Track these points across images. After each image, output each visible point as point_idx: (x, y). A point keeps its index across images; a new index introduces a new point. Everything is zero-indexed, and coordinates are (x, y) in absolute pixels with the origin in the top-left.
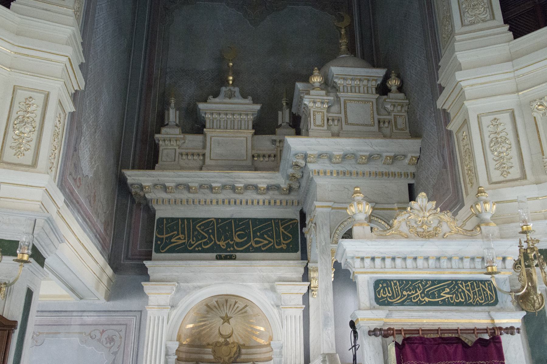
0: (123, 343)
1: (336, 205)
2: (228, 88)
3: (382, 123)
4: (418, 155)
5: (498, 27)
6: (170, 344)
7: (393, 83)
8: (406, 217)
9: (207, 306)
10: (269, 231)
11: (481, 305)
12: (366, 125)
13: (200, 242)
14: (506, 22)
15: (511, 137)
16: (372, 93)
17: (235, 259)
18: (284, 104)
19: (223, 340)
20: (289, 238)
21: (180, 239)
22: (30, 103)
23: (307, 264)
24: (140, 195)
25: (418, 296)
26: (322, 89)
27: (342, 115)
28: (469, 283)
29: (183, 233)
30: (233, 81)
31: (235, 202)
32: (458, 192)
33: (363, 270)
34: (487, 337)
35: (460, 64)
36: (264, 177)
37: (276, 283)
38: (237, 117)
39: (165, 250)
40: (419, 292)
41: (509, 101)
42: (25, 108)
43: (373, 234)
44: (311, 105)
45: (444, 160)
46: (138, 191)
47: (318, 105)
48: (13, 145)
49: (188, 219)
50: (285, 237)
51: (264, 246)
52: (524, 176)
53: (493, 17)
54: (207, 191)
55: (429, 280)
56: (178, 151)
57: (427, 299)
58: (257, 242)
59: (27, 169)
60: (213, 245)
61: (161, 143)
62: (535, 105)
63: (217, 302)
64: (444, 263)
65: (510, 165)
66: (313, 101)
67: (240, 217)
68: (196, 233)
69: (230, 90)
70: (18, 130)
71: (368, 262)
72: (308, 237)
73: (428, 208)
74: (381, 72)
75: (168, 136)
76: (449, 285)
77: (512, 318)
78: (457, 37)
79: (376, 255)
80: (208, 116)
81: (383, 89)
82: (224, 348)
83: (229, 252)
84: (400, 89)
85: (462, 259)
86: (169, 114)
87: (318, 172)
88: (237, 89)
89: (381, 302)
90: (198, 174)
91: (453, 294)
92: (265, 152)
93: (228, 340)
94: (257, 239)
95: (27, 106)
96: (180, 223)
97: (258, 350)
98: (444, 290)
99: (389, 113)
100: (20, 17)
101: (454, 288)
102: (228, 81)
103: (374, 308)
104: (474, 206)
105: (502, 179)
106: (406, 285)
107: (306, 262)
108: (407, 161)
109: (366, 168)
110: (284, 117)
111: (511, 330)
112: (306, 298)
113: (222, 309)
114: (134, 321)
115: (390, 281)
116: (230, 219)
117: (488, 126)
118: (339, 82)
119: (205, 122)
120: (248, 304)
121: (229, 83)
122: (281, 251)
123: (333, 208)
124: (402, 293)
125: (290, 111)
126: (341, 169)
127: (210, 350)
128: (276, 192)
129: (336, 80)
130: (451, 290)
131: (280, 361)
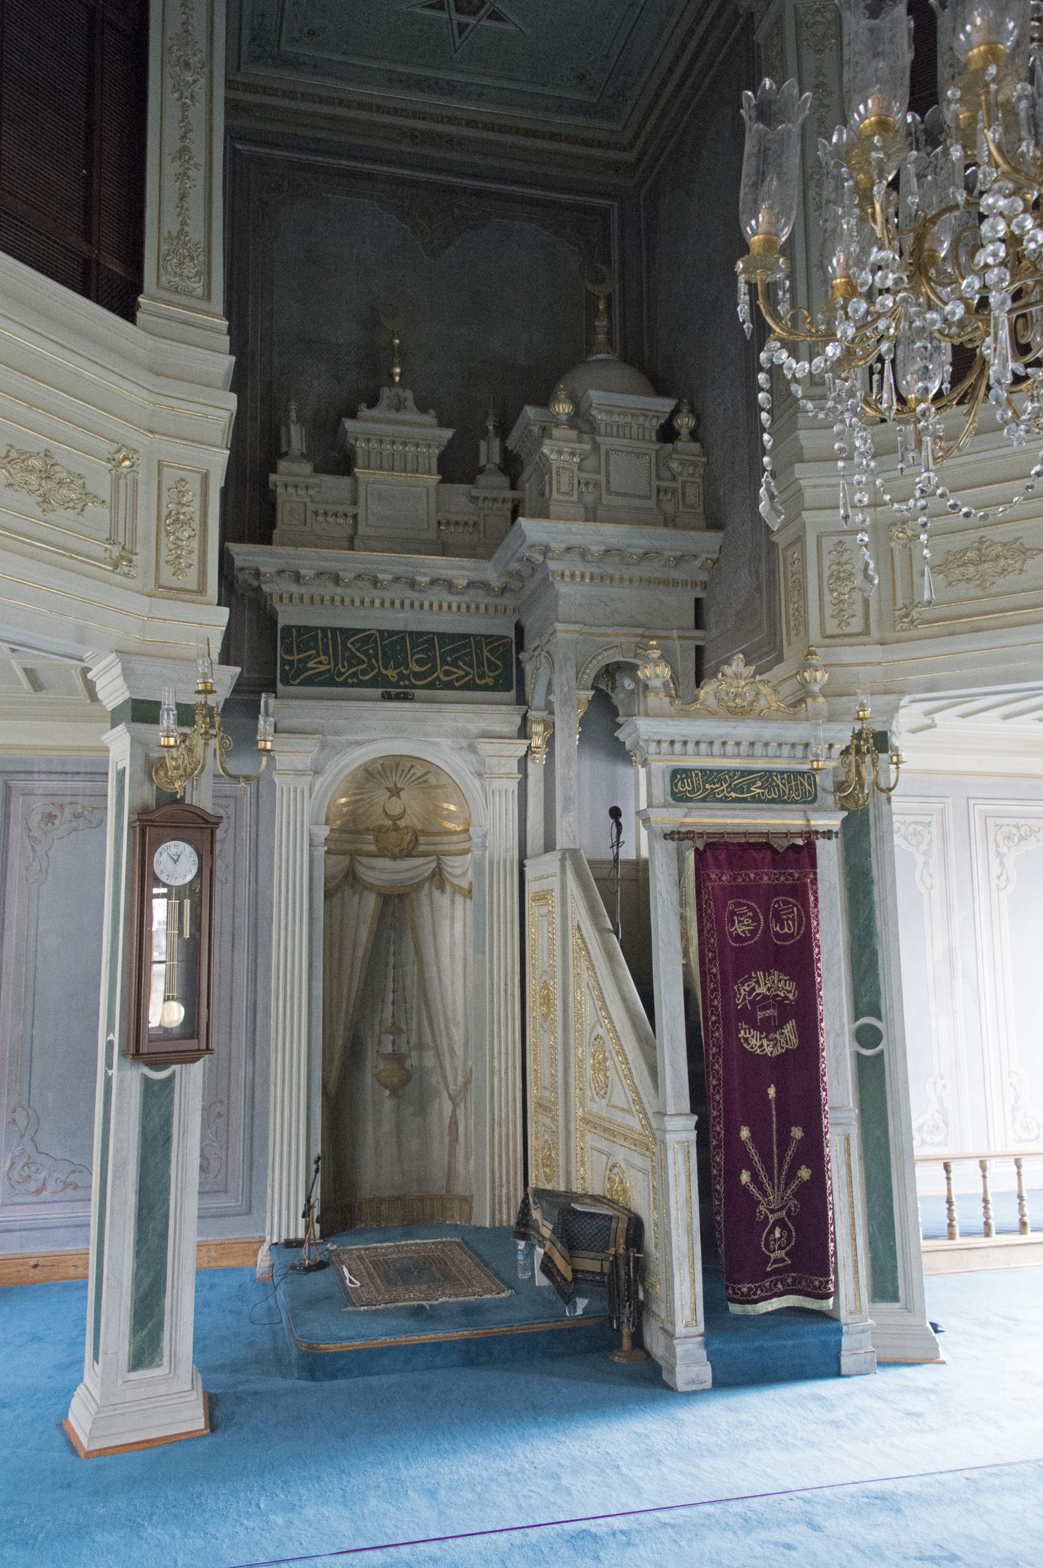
3: (662, 494)
4: (715, 556)
6: (316, 829)
7: (685, 422)
9: (366, 770)
10: (466, 654)
11: (796, 802)
16: (651, 441)
18: (491, 428)
19: (391, 822)
20: (497, 667)
21: (321, 663)
27: (602, 478)
28: (785, 775)
29: (326, 653)
30: (401, 375)
31: (412, 605)
32: (775, 634)
34: (800, 842)
37: (481, 740)
38: (411, 449)
39: (298, 681)
40: (725, 786)
44: (553, 456)
45: (758, 579)
46: (250, 580)
48: (170, 558)
49: (334, 630)
50: (493, 667)
51: (458, 679)
52: (866, 632)
54: (368, 585)
56: (311, 507)
57: (733, 795)
58: (447, 673)
60: (374, 676)
62: (895, 532)
63: (382, 765)
64: (759, 749)
65: (851, 612)
66: (560, 452)
68: (347, 654)
71: (665, 746)
72: (528, 668)
74: (667, 405)
76: (761, 777)
77: (830, 819)
79: (676, 738)
80: (361, 445)
81: (667, 433)
82: (393, 836)
85: (780, 745)
89: (678, 797)
94: (446, 668)
96: (320, 635)
97: (446, 839)
101: (767, 780)
102: (392, 376)
105: (838, 631)
106: (709, 776)
107: (525, 707)
108: (697, 563)
109: (635, 572)
110: (490, 452)
111: (828, 834)
112: (523, 762)
113: (389, 775)
115: (691, 770)
116: (402, 632)
118: (600, 416)
119: (354, 453)
120: (431, 768)
121: (393, 380)
122: (486, 688)
123: (581, 634)
126: (597, 571)
127: (371, 837)
128: (481, 592)
129: (594, 412)
131: (483, 856)
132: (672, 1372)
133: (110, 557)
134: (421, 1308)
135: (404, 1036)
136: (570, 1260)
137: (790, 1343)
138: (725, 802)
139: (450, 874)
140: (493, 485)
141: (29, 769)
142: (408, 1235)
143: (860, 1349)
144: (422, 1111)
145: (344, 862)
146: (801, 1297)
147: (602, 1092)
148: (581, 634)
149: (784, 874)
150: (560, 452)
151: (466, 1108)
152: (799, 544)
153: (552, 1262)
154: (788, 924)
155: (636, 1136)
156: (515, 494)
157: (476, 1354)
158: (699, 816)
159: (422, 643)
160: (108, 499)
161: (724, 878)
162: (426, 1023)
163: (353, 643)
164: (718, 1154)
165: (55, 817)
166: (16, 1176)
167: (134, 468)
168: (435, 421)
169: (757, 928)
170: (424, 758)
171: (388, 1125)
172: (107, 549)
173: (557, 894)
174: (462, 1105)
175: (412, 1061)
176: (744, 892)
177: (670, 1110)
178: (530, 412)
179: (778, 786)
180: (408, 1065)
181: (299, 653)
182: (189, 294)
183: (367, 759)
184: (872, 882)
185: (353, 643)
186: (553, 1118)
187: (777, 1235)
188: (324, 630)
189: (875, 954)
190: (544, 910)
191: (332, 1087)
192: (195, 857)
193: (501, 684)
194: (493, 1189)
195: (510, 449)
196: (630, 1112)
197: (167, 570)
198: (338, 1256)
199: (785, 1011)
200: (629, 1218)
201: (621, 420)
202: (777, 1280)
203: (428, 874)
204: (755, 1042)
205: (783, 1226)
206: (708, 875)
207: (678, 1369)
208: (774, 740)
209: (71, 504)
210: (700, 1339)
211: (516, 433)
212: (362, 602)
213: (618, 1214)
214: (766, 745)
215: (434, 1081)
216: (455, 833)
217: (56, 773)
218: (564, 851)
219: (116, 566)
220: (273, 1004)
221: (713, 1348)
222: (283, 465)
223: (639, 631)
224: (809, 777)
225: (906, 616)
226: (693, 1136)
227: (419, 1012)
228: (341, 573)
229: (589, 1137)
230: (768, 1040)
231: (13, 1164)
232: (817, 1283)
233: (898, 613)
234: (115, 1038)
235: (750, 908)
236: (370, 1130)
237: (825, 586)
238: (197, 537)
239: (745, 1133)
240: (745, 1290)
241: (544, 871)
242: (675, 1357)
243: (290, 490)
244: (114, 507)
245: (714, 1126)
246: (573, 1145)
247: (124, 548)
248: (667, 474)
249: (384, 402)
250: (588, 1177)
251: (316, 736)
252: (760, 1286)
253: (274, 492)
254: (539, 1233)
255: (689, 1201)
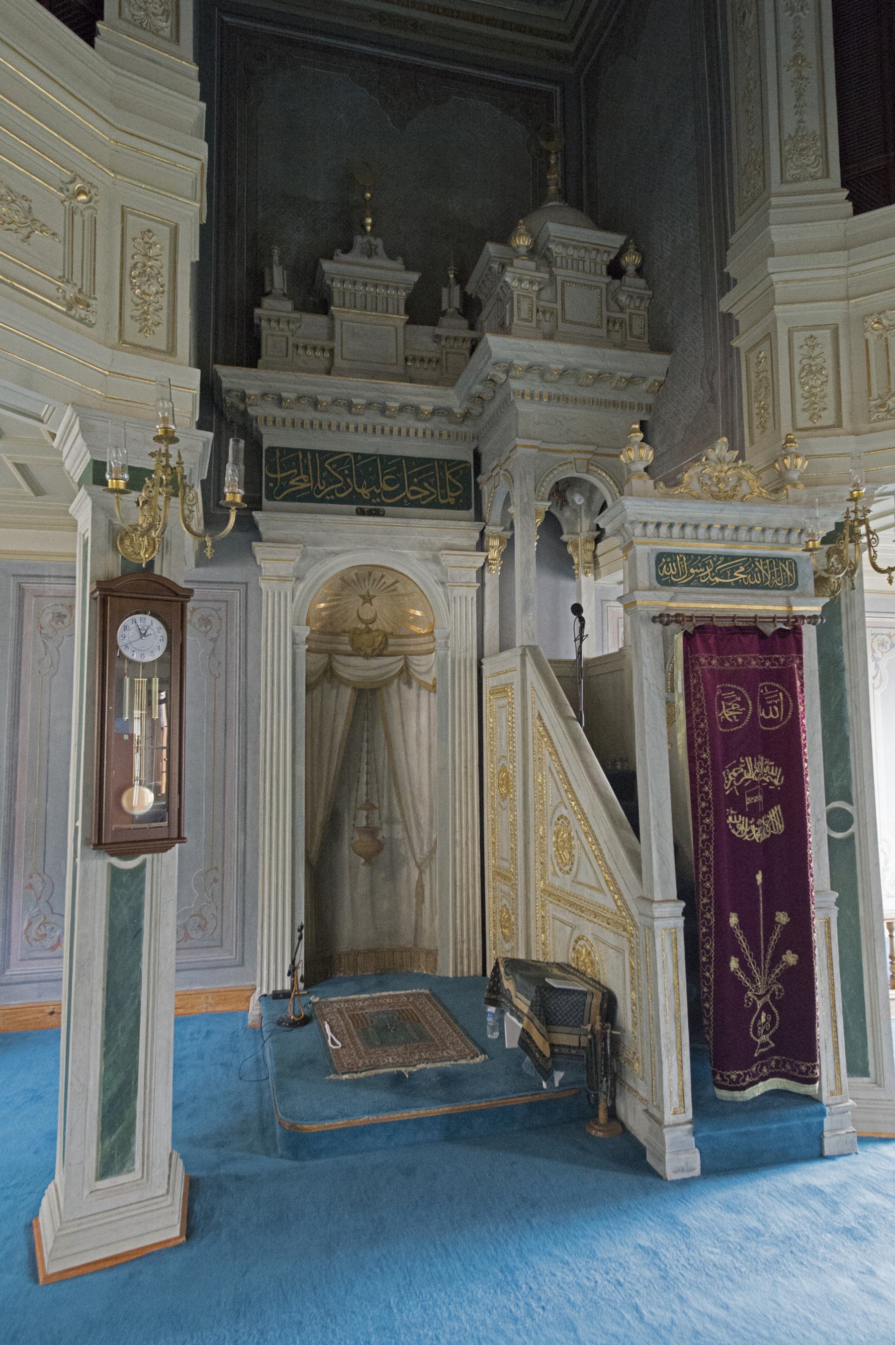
0: (224, 628)
1: (544, 446)
2: (365, 240)
3: (611, 324)
4: (663, 378)
5: (833, 191)
6: (297, 629)
7: (631, 260)
8: (699, 470)
9: (343, 579)
11: (778, 588)
12: (591, 326)
13: (332, 487)
14: (844, 184)
15: (829, 364)
17: (383, 515)
18: (452, 276)
19: (364, 626)
20: (458, 489)
21: (301, 481)
22: (151, 241)
23: (484, 528)
24: (237, 409)
25: (707, 575)
26: (530, 259)
27: (558, 306)
28: (767, 561)
29: (306, 473)
30: (372, 225)
31: (383, 431)
33: (645, 539)
35: (772, 245)
36: (430, 395)
40: (709, 571)
41: (832, 312)
42: (144, 249)
43: (656, 491)
44: (515, 284)
46: (236, 401)
47: (526, 285)
49: (313, 452)
50: (454, 488)
51: (424, 498)
52: (839, 424)
53: (827, 175)
55: (721, 556)
56: (291, 341)
57: (718, 580)
58: (414, 493)
59: (163, 357)
61: (264, 324)
63: (356, 574)
64: (743, 534)
65: (822, 405)
66: (520, 279)
67: (388, 453)
68: (325, 474)
69: (369, 241)
70: (139, 288)
71: (651, 528)
72: (485, 489)
73: (728, 459)
74: (616, 240)
75: (276, 313)
76: (744, 563)
77: (812, 605)
78: (774, 201)
79: (662, 519)
80: (337, 285)
82: (366, 636)
83: (374, 505)
84: (639, 271)
86: (272, 274)
87: (523, 394)
88: (379, 242)
89: (664, 581)
90: (332, 381)
91: (748, 574)
92: (424, 354)
93: (370, 626)
94: (412, 488)
95: (147, 246)
96: (301, 457)
98: (738, 569)
99: (622, 309)
100: (115, 72)
101: (750, 566)
102: (363, 226)
103: (655, 589)
104: (780, 459)
105: (809, 424)
107: (483, 524)
108: (644, 387)
110: (450, 298)
113: (362, 584)
114: (237, 597)
115: (676, 554)
117: (801, 347)
119: (331, 296)
122: (448, 506)
123: (540, 450)
124: (689, 570)
125: (462, 289)
126: (554, 391)
128: (444, 419)
129: (551, 246)
130: (746, 570)
131: (446, 655)
132: (661, 1159)
133: (64, 298)
134: (400, 1075)
135: (376, 812)
136: (547, 1035)
137: (775, 1126)
138: (708, 586)
139: (415, 670)
140: (453, 326)
141: (39, 573)
142: (382, 985)
143: (841, 1129)
144: (393, 875)
145: (322, 659)
146: (784, 1080)
147: (567, 868)
148: (540, 450)
149: (770, 659)
150: (521, 281)
151: (431, 874)
152: (767, 343)
153: (530, 1037)
154: (773, 710)
155: (609, 915)
156: (473, 334)
157: (454, 1129)
158: (684, 601)
159: (391, 466)
160: (61, 233)
161: (714, 662)
162: (395, 801)
163: (330, 464)
164: (708, 941)
165: (65, 616)
166: (33, 935)
167: (92, 204)
168: (403, 267)
169: (745, 713)
170: (395, 568)
171: (363, 888)
172: (59, 288)
173: (517, 687)
174: (428, 871)
175: (383, 834)
176: (734, 676)
177: (658, 896)
178: (491, 248)
179: (760, 571)
180: (379, 837)
181: (283, 470)
182: (156, 32)
183: (343, 568)
184: (844, 669)
185: (330, 464)
186: (514, 887)
187: (763, 1020)
188: (304, 451)
189: (846, 739)
190: (504, 702)
191: (314, 855)
192: (163, 633)
193: (461, 504)
194: (455, 944)
195: (469, 293)
196: (600, 890)
197: (131, 327)
198: (321, 1009)
199: (771, 797)
200: (603, 994)
201: (576, 254)
202: (762, 1065)
203: (396, 671)
204: (744, 828)
205: (766, 1008)
206: (698, 659)
207: (668, 1157)
208: (759, 524)
209: (13, 226)
210: (689, 1126)
211: (475, 275)
212: (338, 427)
213: (591, 988)
214: (751, 529)
215: (402, 850)
216: (420, 635)
217: (65, 577)
218: (524, 648)
219: (70, 308)
220: (261, 783)
221: (700, 1135)
222: (267, 302)
223: (591, 448)
224: (790, 564)
225: (882, 405)
226: (680, 922)
227: (389, 790)
228: (319, 397)
229: (550, 907)
230: (757, 826)
231: (30, 924)
232: (804, 1068)
233: (874, 403)
234: (79, 824)
235: (738, 693)
236: (347, 892)
237: (797, 381)
238: (166, 294)
239: (733, 920)
240: (734, 1077)
241: (502, 668)
242: (663, 1144)
243: (273, 324)
244: (70, 243)
245: (703, 913)
246: (532, 913)
247: (80, 291)
248: (614, 306)
249: (356, 250)
250: (551, 940)
251: (297, 546)
252: (748, 1073)
253: (259, 326)
254: (511, 1002)
255: (676, 986)
